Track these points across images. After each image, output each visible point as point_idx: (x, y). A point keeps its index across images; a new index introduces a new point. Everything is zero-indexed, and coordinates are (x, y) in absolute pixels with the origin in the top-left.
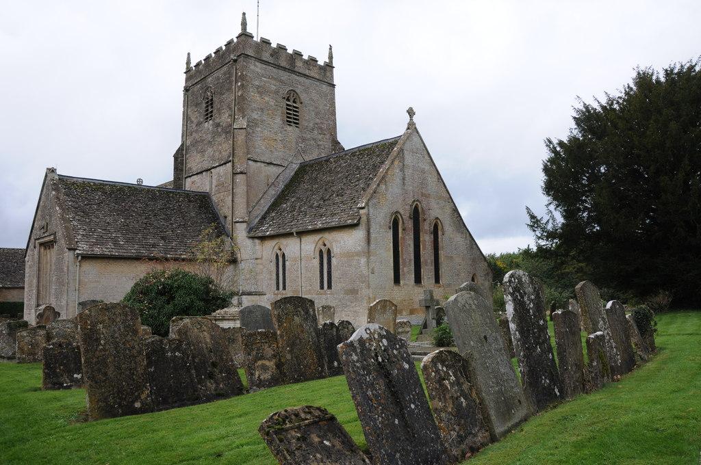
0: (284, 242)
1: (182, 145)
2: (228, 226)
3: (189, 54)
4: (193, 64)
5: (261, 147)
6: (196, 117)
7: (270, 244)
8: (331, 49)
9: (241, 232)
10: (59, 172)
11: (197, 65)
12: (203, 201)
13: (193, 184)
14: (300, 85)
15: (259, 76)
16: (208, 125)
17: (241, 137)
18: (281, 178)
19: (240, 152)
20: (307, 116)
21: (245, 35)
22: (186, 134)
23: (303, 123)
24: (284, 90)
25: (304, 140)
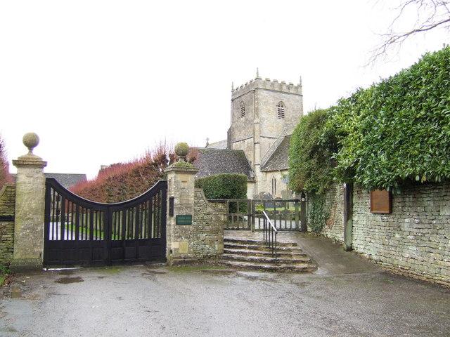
0: (276, 173)
2: (252, 166)
4: (235, 88)
6: (237, 114)
7: (270, 175)
9: (258, 169)
13: (235, 146)
16: (243, 119)
17: (257, 127)
19: (257, 133)
22: (233, 121)
23: (286, 116)
24: (277, 103)
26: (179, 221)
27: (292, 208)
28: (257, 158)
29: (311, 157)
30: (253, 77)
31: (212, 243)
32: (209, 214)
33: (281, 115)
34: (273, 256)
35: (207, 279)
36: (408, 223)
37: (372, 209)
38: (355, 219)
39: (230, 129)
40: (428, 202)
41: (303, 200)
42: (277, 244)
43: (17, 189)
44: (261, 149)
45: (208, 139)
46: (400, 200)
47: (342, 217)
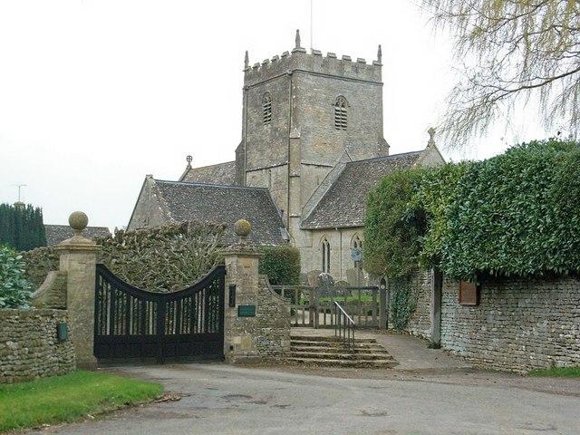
0: (329, 234)
1: (243, 142)
3: (247, 52)
4: (251, 64)
5: (311, 152)
6: (256, 117)
7: (318, 236)
8: (380, 52)
9: (295, 226)
10: (155, 178)
11: (255, 68)
12: (262, 195)
14: (347, 89)
15: (311, 88)
16: (267, 128)
17: (295, 146)
18: (330, 177)
20: (354, 119)
21: (298, 51)
22: (246, 131)
23: (350, 125)
24: (333, 99)
25: (351, 140)
26: (242, 313)
27: (367, 298)
28: (296, 205)
29: (394, 234)
30: (290, 47)
31: (277, 338)
32: (274, 304)
33: (340, 123)
34: (350, 352)
35: (237, 417)
36: (493, 314)
37: (460, 301)
38: (444, 311)
39: (241, 146)
40: (509, 294)
41: (383, 287)
42: (353, 340)
43: (69, 277)
44: (302, 186)
45: (189, 159)
46: (487, 291)
47: (431, 309)
